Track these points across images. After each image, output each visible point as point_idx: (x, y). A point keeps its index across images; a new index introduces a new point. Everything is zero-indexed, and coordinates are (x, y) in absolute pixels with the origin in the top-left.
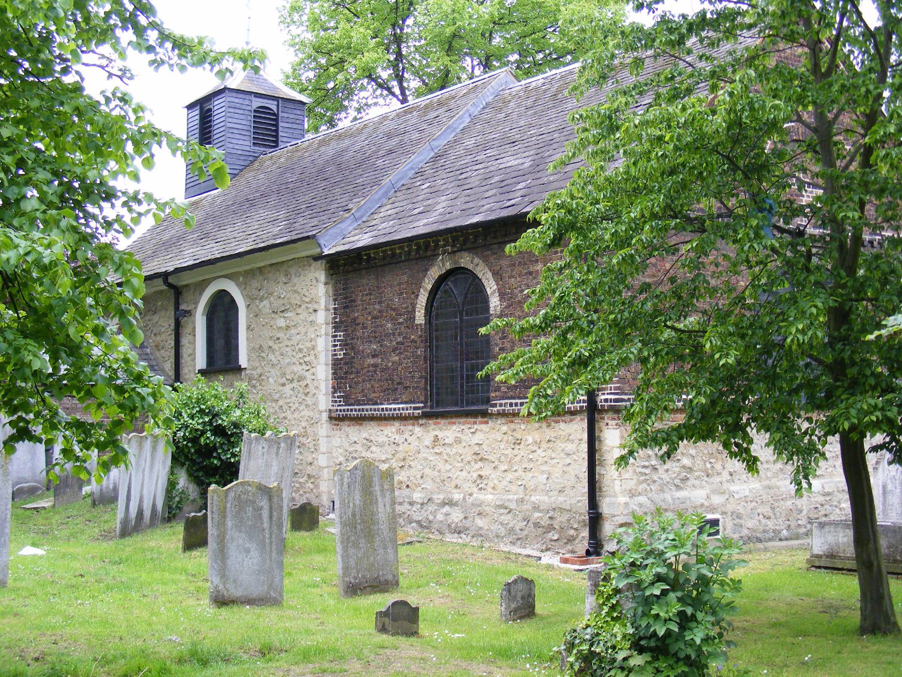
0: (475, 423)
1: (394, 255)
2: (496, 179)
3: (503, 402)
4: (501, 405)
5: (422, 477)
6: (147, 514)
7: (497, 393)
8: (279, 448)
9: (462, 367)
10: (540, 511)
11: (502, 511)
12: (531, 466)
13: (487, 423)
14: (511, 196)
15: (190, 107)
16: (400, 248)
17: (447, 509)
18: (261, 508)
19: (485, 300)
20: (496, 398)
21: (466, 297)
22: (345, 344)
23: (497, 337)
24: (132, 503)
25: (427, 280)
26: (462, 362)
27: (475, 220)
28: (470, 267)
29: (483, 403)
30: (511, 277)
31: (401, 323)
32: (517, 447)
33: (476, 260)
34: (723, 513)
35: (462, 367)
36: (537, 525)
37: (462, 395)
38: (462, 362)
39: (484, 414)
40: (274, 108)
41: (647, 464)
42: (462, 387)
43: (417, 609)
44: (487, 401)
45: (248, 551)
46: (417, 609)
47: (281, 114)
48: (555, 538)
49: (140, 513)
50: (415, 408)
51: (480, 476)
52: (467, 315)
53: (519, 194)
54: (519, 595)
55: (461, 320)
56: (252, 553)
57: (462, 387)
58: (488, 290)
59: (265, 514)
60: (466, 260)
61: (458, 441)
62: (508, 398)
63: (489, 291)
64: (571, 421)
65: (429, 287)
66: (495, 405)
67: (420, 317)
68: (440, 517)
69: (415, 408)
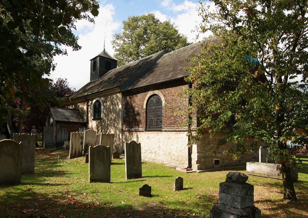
0: (158, 133)
1: (138, 91)
2: (164, 73)
3: (166, 128)
4: (165, 129)
5: (145, 146)
6: (77, 152)
7: (164, 126)
8: (110, 137)
9: (155, 119)
10: (175, 156)
11: (165, 155)
12: (173, 144)
13: (161, 133)
14: (169, 76)
15: (91, 60)
16: (140, 89)
17: (151, 154)
18: (104, 153)
19: (161, 102)
20: (164, 127)
21: (156, 102)
22: (126, 113)
23: (164, 112)
24: (73, 150)
25: (146, 97)
26: (155, 118)
27: (159, 82)
28: (158, 94)
29: (160, 128)
30: (168, 96)
31: (140, 108)
32: (169, 139)
33: (159, 92)
34: (220, 159)
35: (155, 119)
36: (174, 159)
37: (155, 126)
38: (155, 118)
39: (161, 131)
40: (110, 61)
41: (203, 145)
42: (155, 124)
43: (151, 187)
44: (161, 127)
45: (100, 166)
46: (151, 187)
47: (111, 63)
48: (179, 163)
49: (75, 152)
50: (143, 129)
51: (159, 146)
52: (156, 106)
53: (170, 75)
54: (179, 182)
55: (155, 107)
56: (101, 166)
57: (155, 124)
58: (162, 100)
59: (105, 155)
60: (156, 92)
61: (154, 137)
62: (167, 127)
63: (162, 100)
64: (183, 133)
65: (147, 99)
66: (164, 129)
67: (145, 107)
68: (149, 156)
69: (143, 129)
